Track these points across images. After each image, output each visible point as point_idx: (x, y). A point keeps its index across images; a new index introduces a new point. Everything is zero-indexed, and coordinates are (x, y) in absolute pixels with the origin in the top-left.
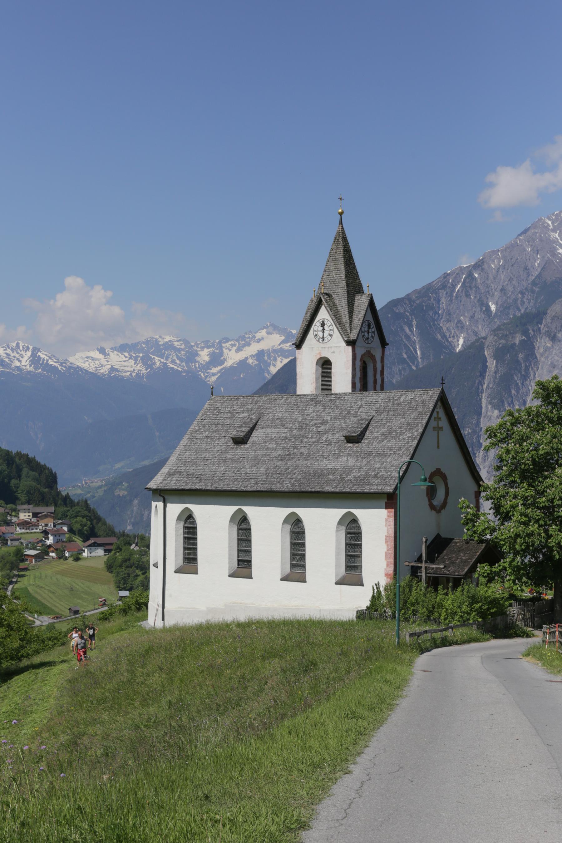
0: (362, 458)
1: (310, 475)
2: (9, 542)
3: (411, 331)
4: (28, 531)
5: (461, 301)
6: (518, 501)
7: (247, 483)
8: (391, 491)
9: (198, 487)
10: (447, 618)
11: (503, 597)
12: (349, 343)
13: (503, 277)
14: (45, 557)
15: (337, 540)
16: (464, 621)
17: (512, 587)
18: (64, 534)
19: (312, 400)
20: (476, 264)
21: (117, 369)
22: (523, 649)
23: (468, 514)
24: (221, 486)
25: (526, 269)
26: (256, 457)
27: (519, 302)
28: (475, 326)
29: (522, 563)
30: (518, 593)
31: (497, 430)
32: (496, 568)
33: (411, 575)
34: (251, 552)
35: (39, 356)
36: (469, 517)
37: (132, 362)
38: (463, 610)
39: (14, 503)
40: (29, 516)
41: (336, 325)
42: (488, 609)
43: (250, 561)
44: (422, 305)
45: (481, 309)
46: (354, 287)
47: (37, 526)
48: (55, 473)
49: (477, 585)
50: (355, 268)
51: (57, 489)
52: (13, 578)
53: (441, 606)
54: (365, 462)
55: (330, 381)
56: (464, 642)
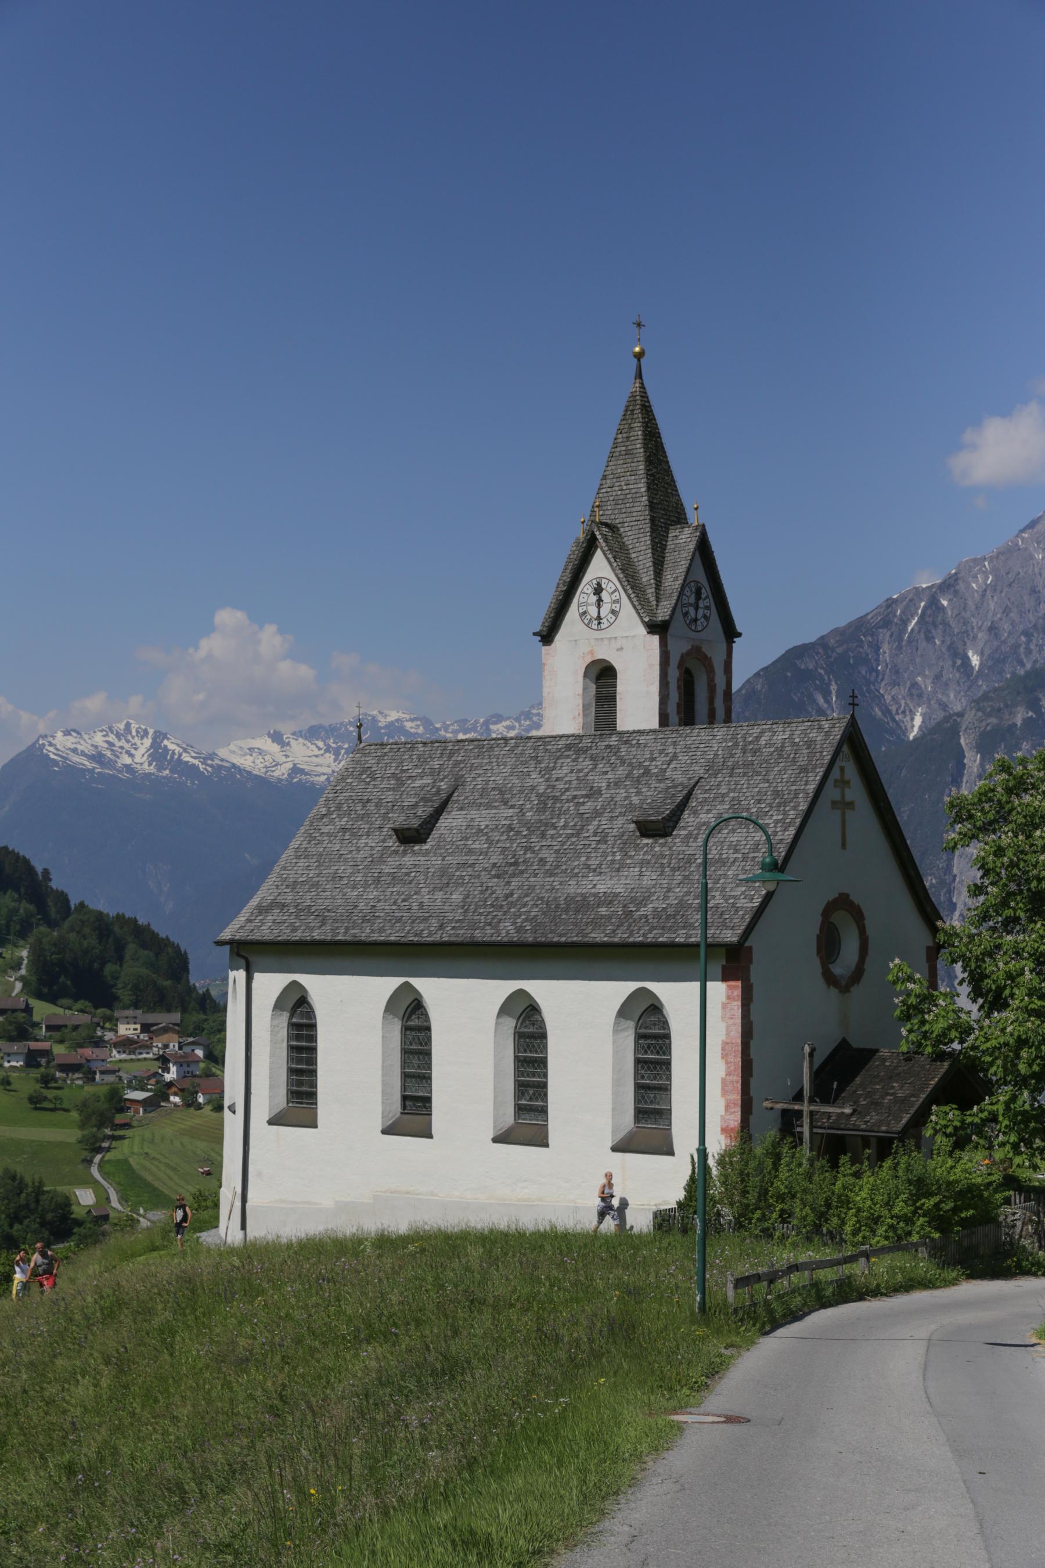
0: (673, 870)
1: (557, 906)
2: (98, 1077)
3: (828, 701)
4: (133, 1057)
5: (917, 649)
6: (1024, 962)
7: (422, 926)
8: (735, 939)
9: (317, 935)
10: (859, 1229)
11: (990, 1184)
12: (653, 628)
13: (992, 606)
14: (163, 1104)
16: (900, 1238)
17: (1011, 1159)
18: (197, 1062)
19: (568, 747)
20: (944, 582)
21: (303, 770)
23: (909, 995)
24: (366, 933)
25: (1034, 591)
26: (443, 871)
27: (1022, 650)
28: (943, 694)
29: (1032, 1105)
30: (1025, 1174)
31: (974, 804)
32: (975, 1114)
33: (781, 1130)
34: (430, 1078)
35: (166, 746)
36: (912, 1000)
37: (330, 758)
38: (896, 1211)
39: (110, 1007)
40: (135, 1029)
41: (625, 591)
42: (956, 1210)
43: (428, 1100)
45: (954, 663)
46: (666, 509)
47: (148, 1047)
48: (185, 953)
49: (930, 1155)
50: (668, 471)
51: (188, 981)
52: (103, 1141)
53: (845, 1202)
55: (613, 712)
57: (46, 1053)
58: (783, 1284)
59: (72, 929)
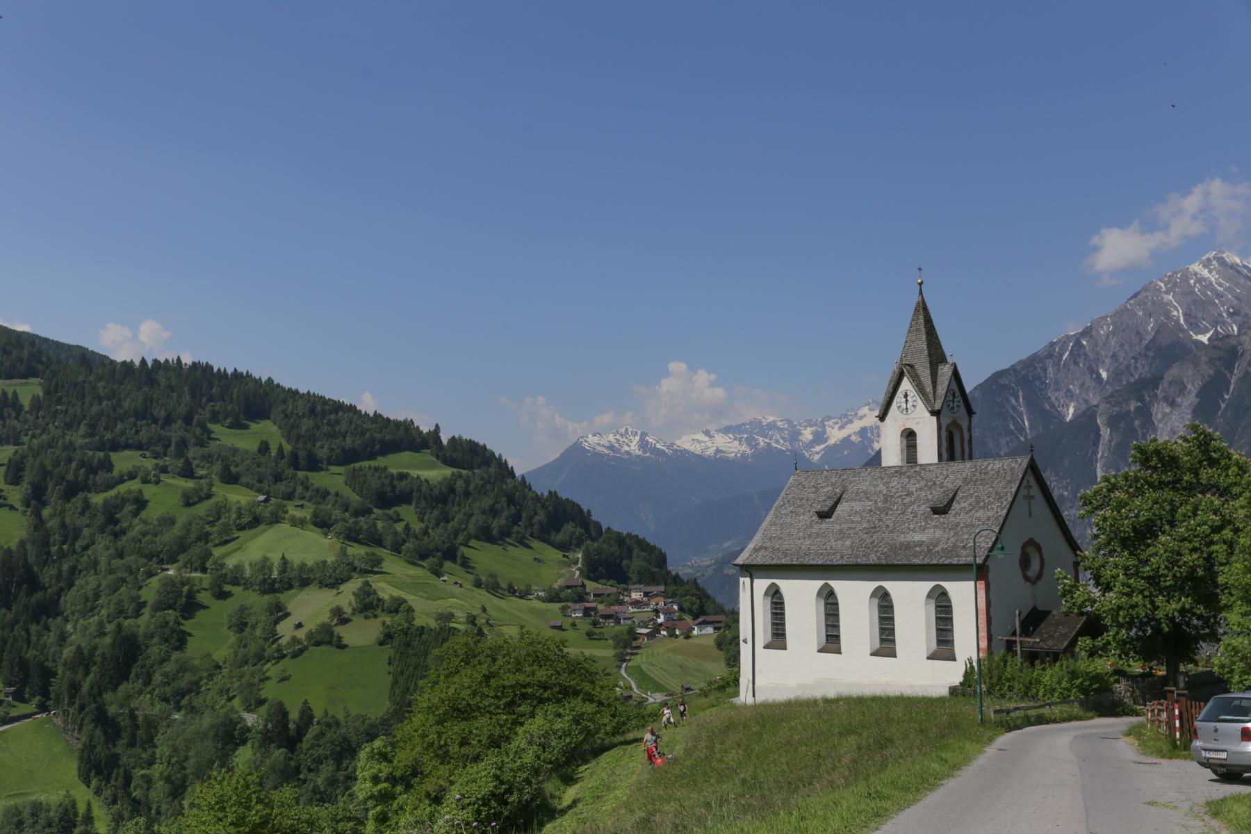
9: (783, 562)
12: (933, 413)
15: (927, 614)
22: (1125, 728)
24: (807, 561)
25: (1138, 333)
26: (841, 531)
32: (1099, 642)
37: (737, 443)
42: (1091, 685)
43: (838, 636)
44: (1027, 378)
46: (936, 356)
47: (648, 605)
53: (1039, 682)
54: (952, 533)
56: (1064, 720)
57: (594, 609)
58: (1013, 715)
59: (604, 542)
